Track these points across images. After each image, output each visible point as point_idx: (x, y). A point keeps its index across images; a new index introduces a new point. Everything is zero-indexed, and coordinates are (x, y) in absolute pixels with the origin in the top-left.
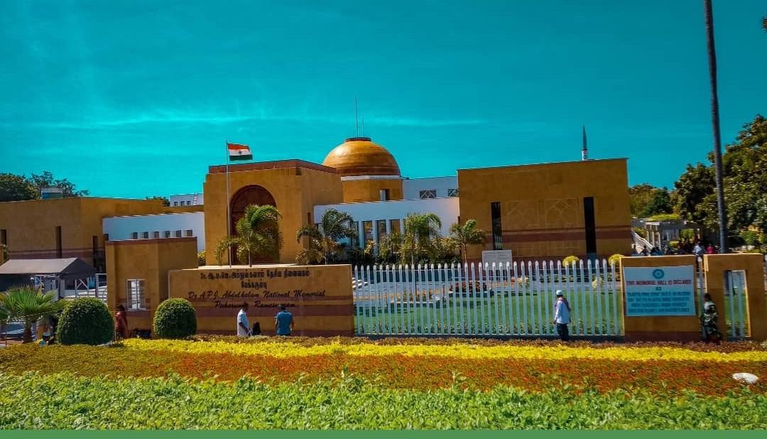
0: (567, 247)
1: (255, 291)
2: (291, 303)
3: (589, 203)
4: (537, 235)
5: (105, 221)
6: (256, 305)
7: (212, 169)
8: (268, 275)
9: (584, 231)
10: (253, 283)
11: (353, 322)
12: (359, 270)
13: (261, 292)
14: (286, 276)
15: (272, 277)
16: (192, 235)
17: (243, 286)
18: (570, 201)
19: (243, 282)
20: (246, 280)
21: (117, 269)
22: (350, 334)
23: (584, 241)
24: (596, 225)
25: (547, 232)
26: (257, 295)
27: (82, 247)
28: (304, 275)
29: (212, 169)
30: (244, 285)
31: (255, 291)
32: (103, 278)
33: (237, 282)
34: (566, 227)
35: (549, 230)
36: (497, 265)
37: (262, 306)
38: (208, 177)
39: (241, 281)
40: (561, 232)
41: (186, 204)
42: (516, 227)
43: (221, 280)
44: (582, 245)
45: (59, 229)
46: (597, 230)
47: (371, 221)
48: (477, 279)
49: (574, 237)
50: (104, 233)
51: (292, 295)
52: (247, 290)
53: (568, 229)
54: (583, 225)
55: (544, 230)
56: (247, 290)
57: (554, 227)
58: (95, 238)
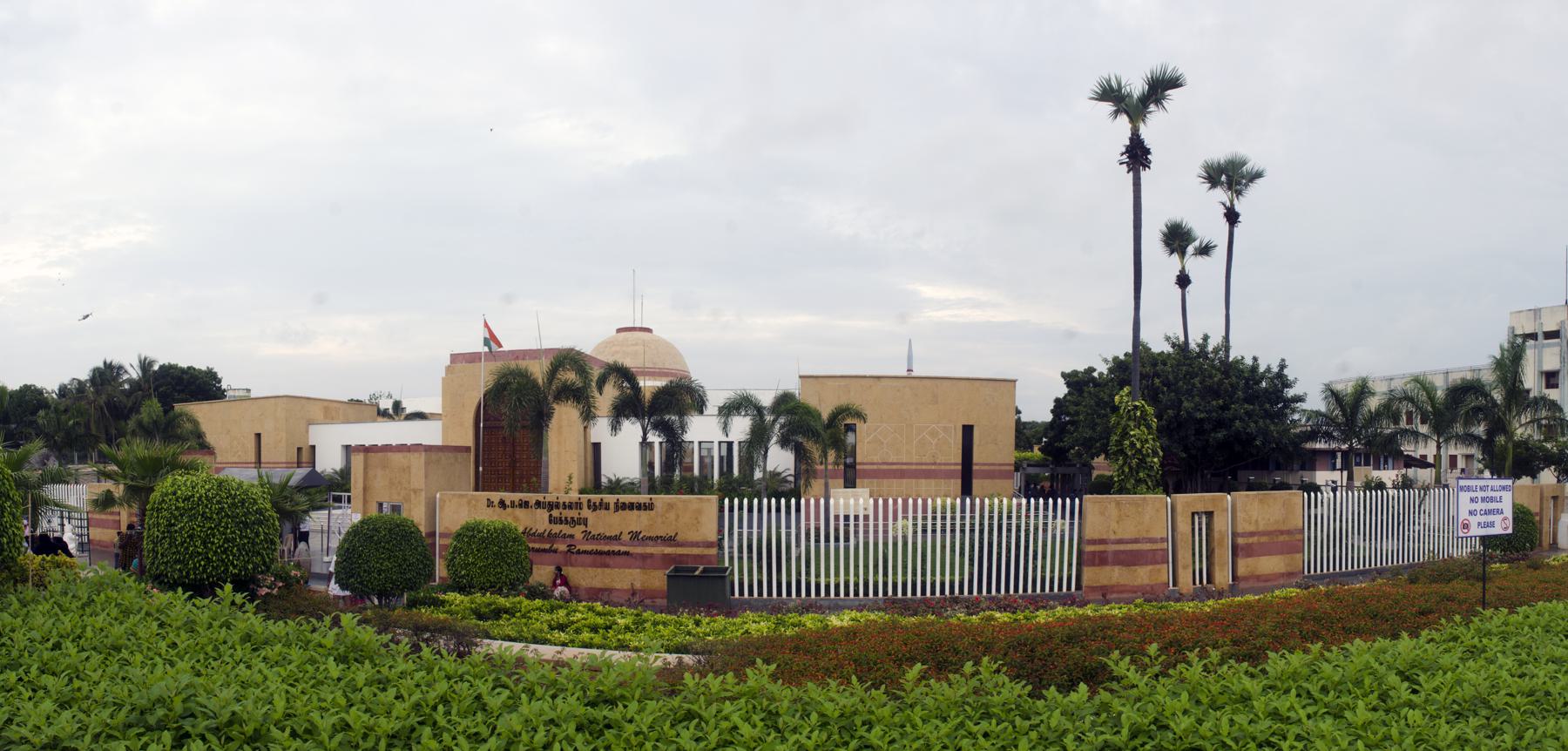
1: (566, 529)
2: (623, 549)
3: (968, 431)
4: (902, 470)
5: (312, 429)
6: (569, 551)
8: (589, 507)
9: (960, 467)
10: (566, 518)
11: (1269, 554)
12: (1046, 504)
13: (578, 531)
14: (617, 510)
15: (595, 510)
16: (1356, 465)
17: (550, 522)
18: (945, 429)
19: (551, 516)
21: (365, 489)
22: (731, 610)
23: (959, 481)
25: (914, 467)
26: (572, 536)
27: (284, 461)
30: (552, 520)
31: (566, 529)
33: (543, 515)
34: (938, 461)
35: (917, 464)
37: (579, 552)
38: (448, 369)
39: (548, 514)
40: (933, 467)
42: (876, 459)
44: (956, 484)
45: (258, 436)
46: (975, 468)
47: (693, 442)
49: (948, 475)
50: (311, 443)
51: (626, 537)
52: (556, 528)
53: (940, 464)
54: (959, 460)
55: (911, 464)
56: (556, 528)
57: (924, 461)
58: (299, 449)
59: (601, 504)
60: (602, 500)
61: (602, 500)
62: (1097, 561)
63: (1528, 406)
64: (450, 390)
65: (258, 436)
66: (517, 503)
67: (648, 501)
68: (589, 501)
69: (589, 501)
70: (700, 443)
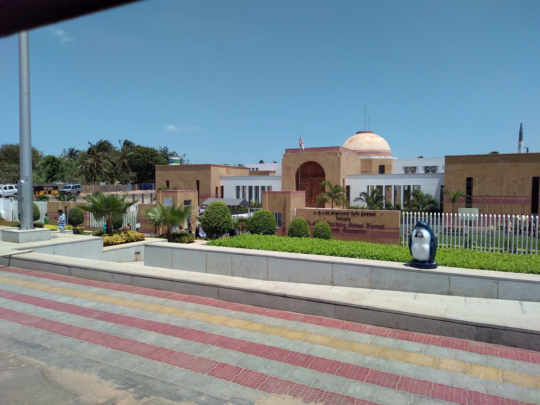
0: (306, 183)
1: (343, 222)
6: (344, 230)
7: (287, 150)
13: (347, 223)
20: (339, 216)
24: (516, 152)
28: (373, 215)
29: (287, 150)
31: (343, 222)
32: (519, 220)
36: (466, 215)
38: (284, 155)
41: (255, 170)
43: (325, 216)
45: (198, 182)
47: (250, 168)
48: (458, 225)
51: (365, 225)
52: (339, 222)
56: (339, 222)
58: (217, 188)
59: (356, 213)
60: (363, 212)
61: (357, 211)
62: (14, 166)
63: (93, 208)
64: (286, 168)
65: (198, 182)
66: (324, 212)
67: (374, 213)
68: (352, 212)
69: (352, 212)
70: (414, 186)
